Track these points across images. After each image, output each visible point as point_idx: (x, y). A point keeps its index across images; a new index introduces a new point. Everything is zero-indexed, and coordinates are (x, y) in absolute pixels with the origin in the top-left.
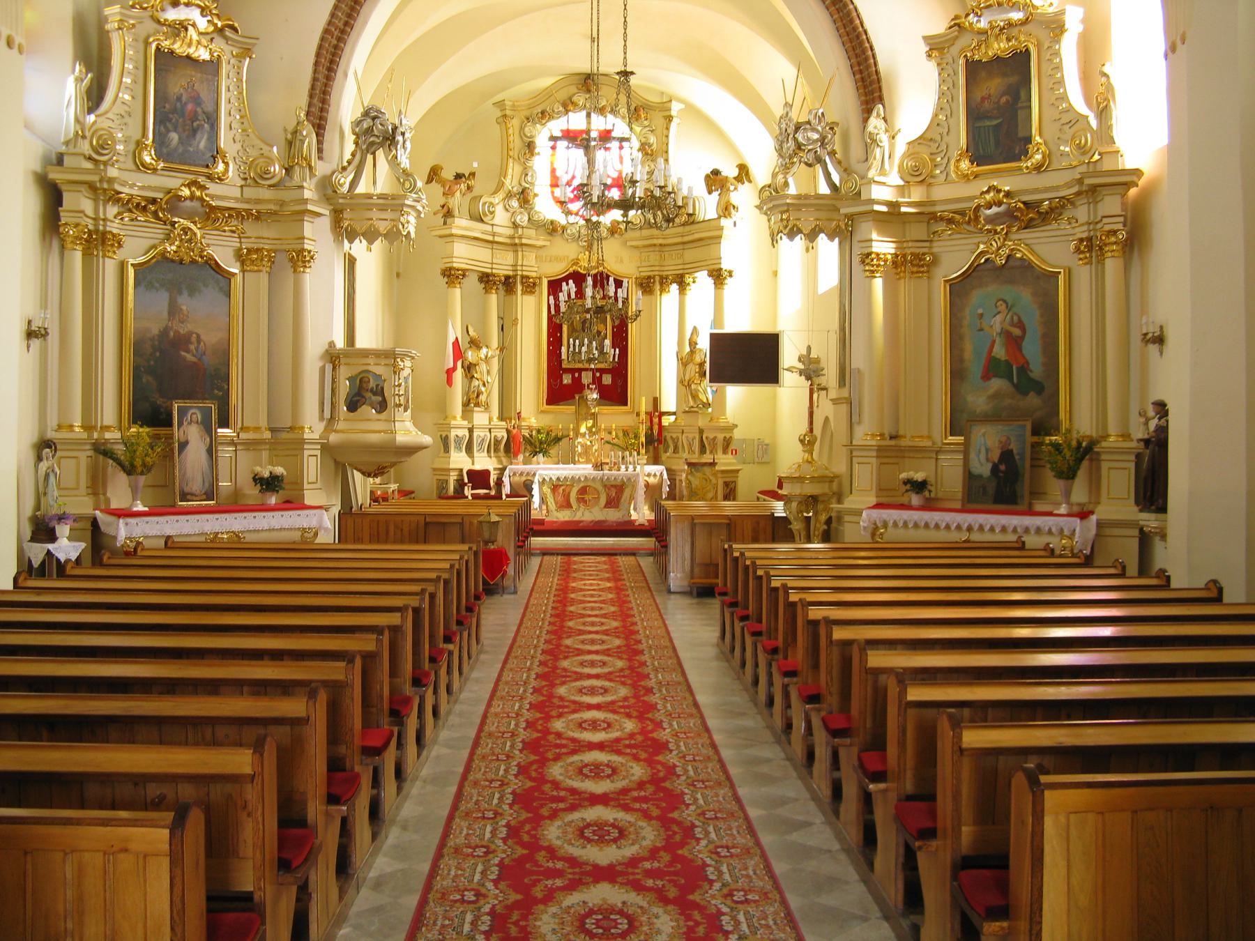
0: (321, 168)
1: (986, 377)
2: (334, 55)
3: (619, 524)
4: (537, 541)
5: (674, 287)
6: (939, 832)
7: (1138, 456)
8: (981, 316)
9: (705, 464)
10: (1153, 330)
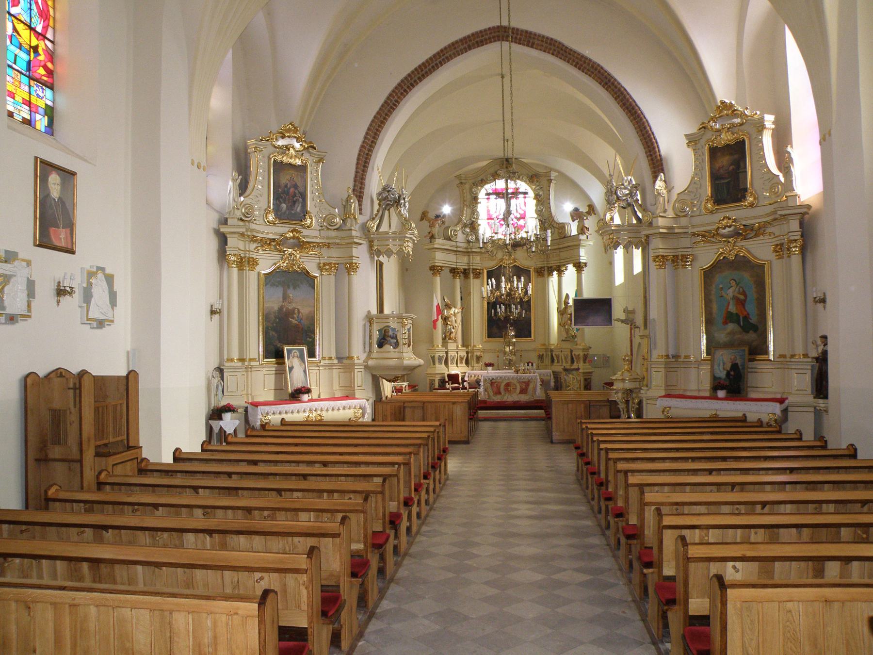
0: (361, 219)
1: (725, 323)
2: (366, 159)
3: (527, 403)
4: (482, 413)
5: (555, 273)
6: (677, 601)
7: (812, 366)
8: (722, 289)
9: (574, 370)
10: (820, 295)
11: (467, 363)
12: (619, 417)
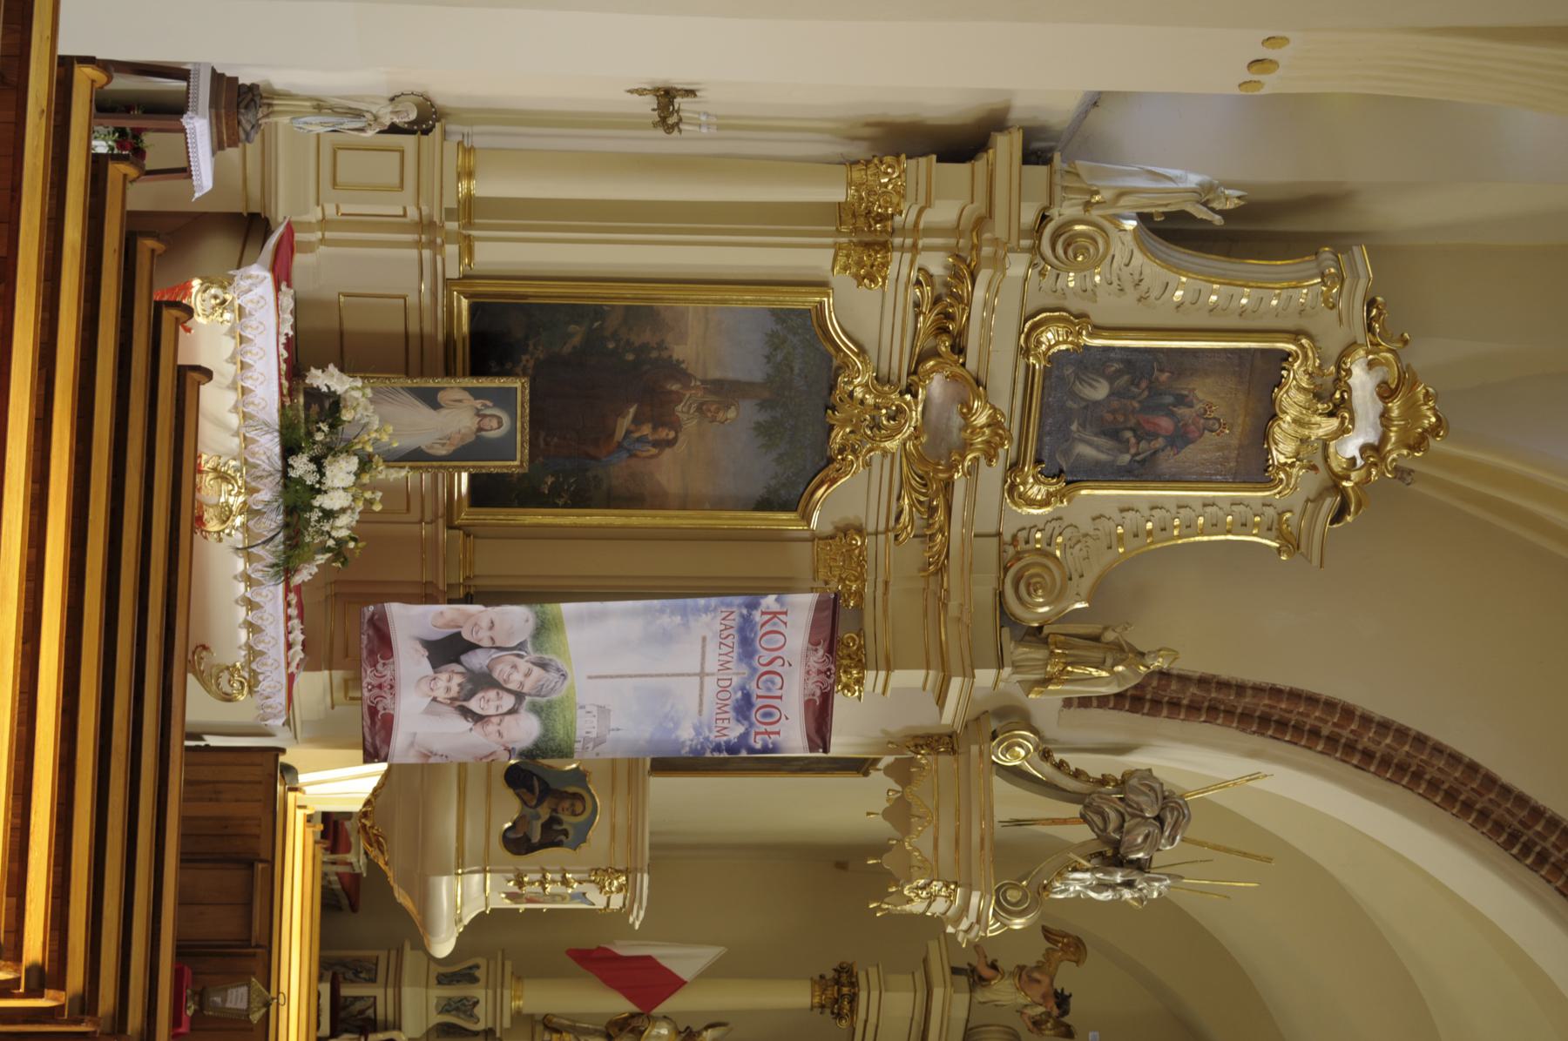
0: (1044, 704)
2: (1298, 729)
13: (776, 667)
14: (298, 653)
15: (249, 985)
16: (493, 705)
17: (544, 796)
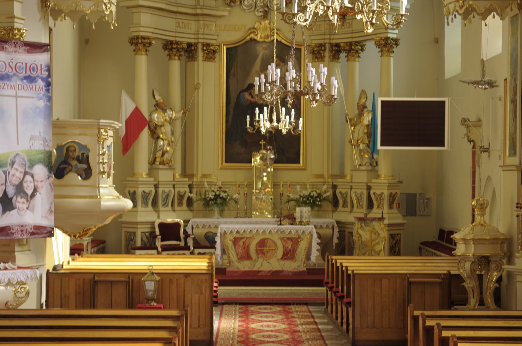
3: (295, 274)
9: (374, 219)
11: (155, 203)
12: (464, 302)
13: (13, 66)
14: (9, 265)
15: (144, 281)
16: (29, 184)
17: (67, 163)
